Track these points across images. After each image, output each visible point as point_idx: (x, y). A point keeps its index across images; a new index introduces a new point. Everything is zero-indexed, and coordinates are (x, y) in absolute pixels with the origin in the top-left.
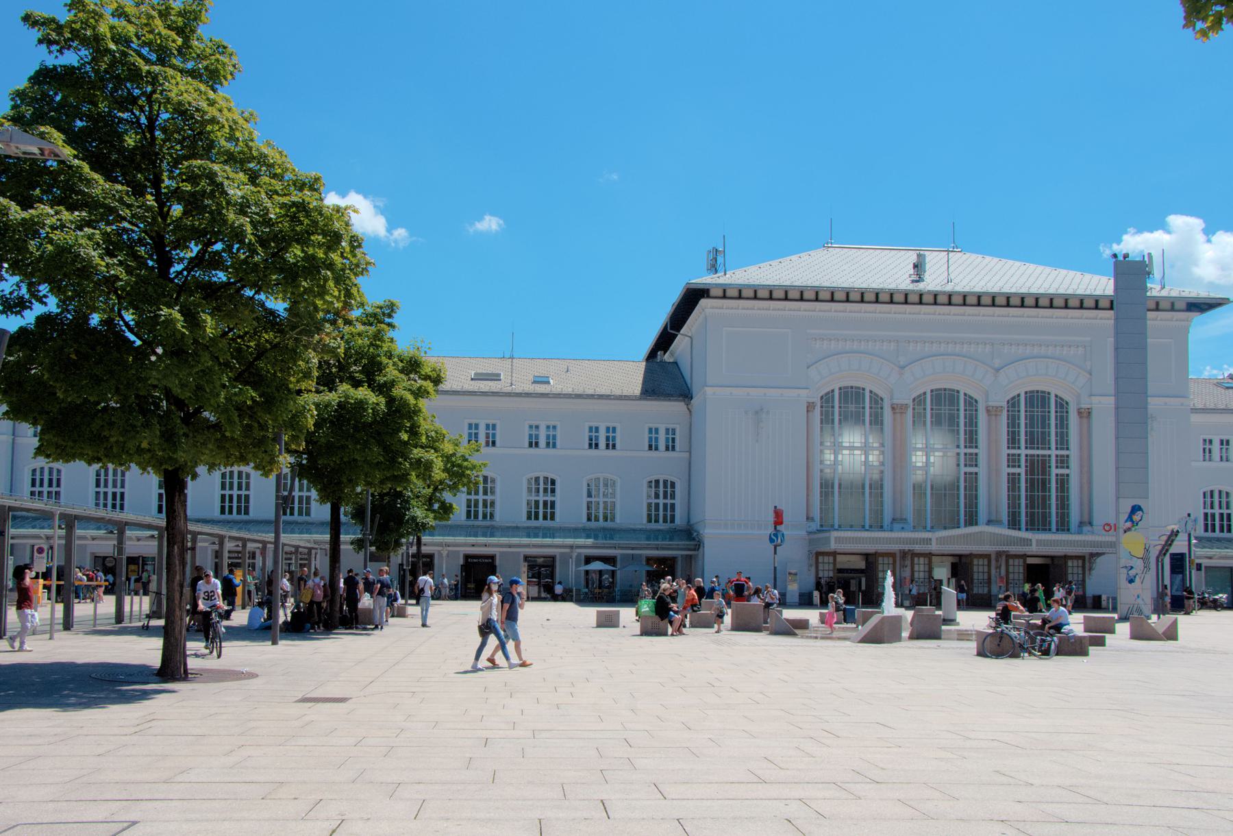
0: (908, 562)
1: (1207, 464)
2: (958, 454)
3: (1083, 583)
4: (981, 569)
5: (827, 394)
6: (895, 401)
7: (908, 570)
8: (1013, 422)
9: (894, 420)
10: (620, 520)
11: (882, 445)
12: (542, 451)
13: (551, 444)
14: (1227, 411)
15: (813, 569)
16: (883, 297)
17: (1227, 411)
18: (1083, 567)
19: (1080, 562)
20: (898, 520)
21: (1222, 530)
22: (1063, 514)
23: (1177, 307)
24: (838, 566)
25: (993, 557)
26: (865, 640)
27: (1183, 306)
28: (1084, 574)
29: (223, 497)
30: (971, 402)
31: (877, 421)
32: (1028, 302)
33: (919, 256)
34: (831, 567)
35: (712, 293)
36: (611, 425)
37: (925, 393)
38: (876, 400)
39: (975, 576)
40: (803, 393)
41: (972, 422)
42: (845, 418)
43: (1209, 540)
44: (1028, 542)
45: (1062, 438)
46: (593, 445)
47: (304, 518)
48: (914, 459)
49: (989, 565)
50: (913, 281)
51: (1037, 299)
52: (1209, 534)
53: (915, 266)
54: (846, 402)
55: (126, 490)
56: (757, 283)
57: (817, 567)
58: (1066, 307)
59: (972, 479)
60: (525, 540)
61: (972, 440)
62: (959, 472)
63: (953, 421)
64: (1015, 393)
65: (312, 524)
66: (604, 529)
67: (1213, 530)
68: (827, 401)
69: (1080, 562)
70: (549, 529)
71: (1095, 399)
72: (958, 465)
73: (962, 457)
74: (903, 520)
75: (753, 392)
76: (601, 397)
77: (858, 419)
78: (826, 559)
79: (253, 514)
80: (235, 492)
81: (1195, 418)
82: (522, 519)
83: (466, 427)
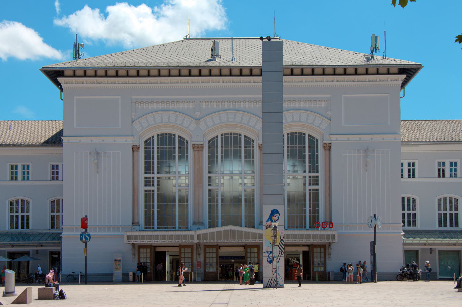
0: (202, 252)
1: (441, 179)
2: (305, 177)
3: (324, 264)
4: (319, 255)
5: (150, 139)
6: (325, 142)
7: (202, 256)
8: (149, 155)
9: (325, 153)
10: (33, 226)
11: (253, 172)
12: (20, 182)
13: (26, 177)
14: (459, 142)
15: (136, 257)
16: (164, 72)
17: (459, 142)
18: (325, 253)
19: (322, 250)
20: (198, 223)
21: (451, 225)
22: (314, 217)
23: (337, 72)
24: (221, 254)
25: (195, 247)
26: (14, 303)
27: (396, 71)
28: (325, 257)
29: (12, 217)
30: (314, 141)
31: (250, 157)
32: (245, 72)
33: (214, 43)
34: (215, 255)
35: (67, 73)
36: (26, 164)
37: (153, 137)
38: (183, 142)
39: (315, 260)
40: (130, 139)
41: (314, 155)
42: (226, 155)
43: (441, 232)
44: (192, 237)
45: (313, 164)
46: (14, 177)
47: (454, 228)
48: (187, 181)
49: (192, 253)
50: (208, 61)
51: (210, 70)
52: (443, 228)
53: (212, 50)
54: (292, 143)
55: (30, 214)
56: (128, 65)
57: (139, 255)
58: (138, 76)
59: (314, 194)
60: (438, 241)
61: (314, 167)
62: (305, 189)
63: (301, 156)
64: (150, 136)
65: (32, 234)
66: (20, 234)
67: (17, 227)
68: (213, 144)
69: (322, 250)
70: (26, 234)
71: (333, 138)
72: (305, 184)
73: (307, 178)
74: (202, 223)
75: (365, 137)
76: (8, 145)
77: (237, 155)
78: (145, 250)
79: (419, 226)
80: (448, 212)
81: (404, 149)
82: (436, 227)
83: (50, 168)
